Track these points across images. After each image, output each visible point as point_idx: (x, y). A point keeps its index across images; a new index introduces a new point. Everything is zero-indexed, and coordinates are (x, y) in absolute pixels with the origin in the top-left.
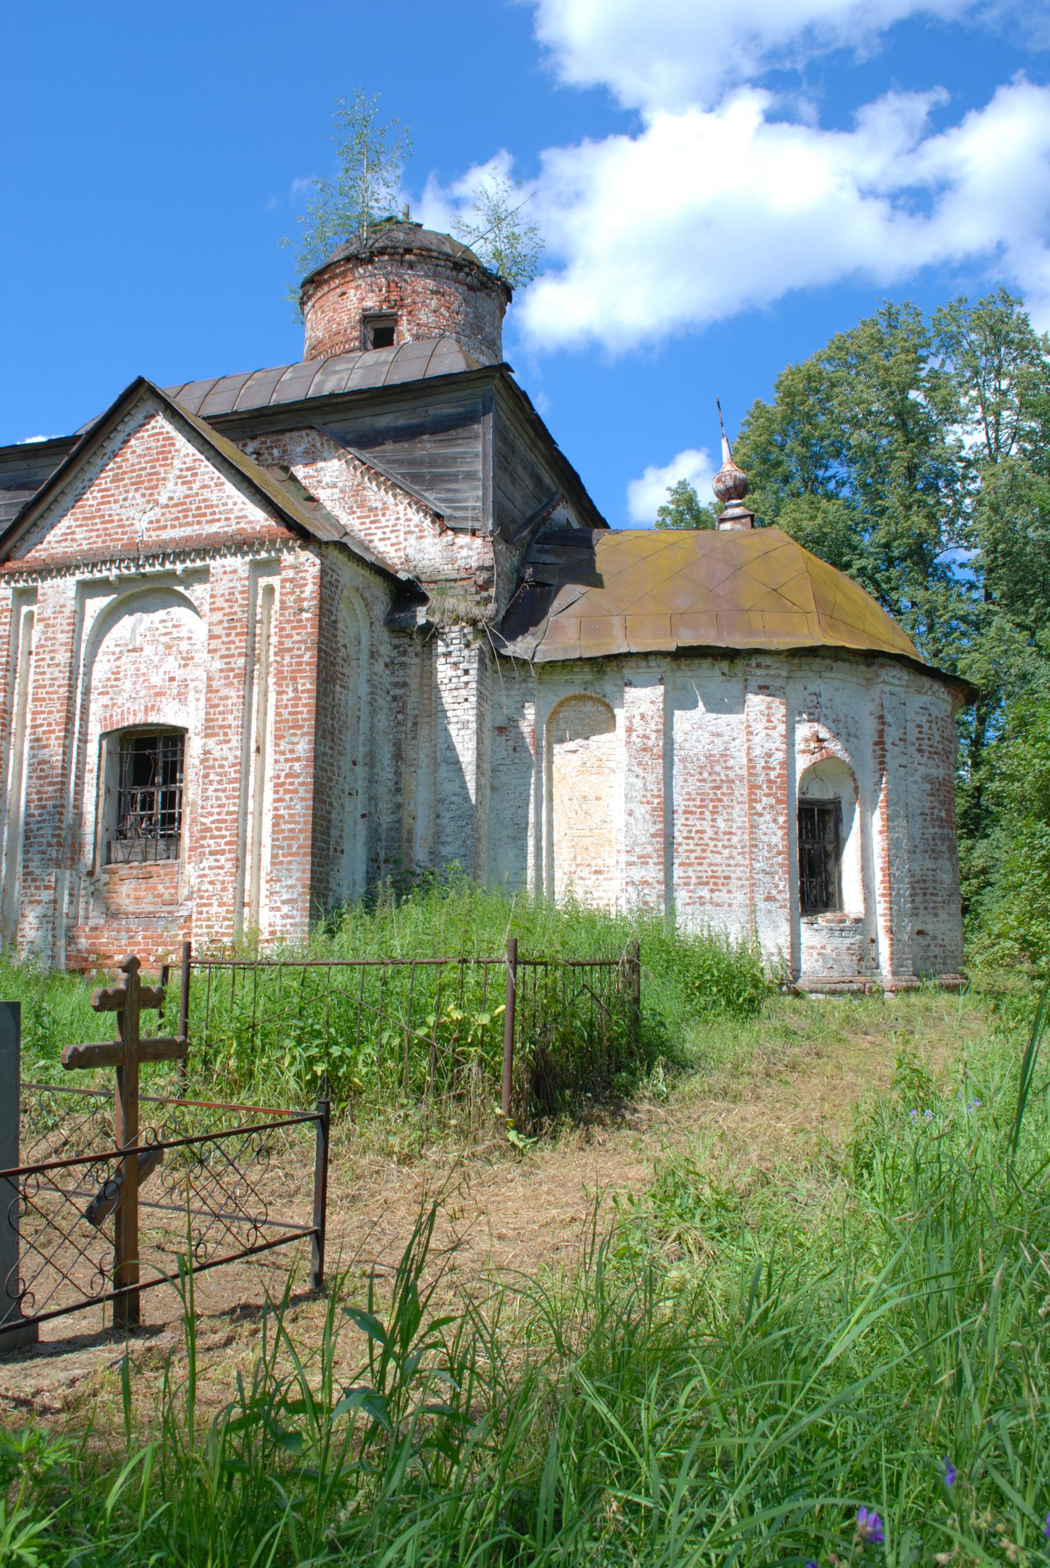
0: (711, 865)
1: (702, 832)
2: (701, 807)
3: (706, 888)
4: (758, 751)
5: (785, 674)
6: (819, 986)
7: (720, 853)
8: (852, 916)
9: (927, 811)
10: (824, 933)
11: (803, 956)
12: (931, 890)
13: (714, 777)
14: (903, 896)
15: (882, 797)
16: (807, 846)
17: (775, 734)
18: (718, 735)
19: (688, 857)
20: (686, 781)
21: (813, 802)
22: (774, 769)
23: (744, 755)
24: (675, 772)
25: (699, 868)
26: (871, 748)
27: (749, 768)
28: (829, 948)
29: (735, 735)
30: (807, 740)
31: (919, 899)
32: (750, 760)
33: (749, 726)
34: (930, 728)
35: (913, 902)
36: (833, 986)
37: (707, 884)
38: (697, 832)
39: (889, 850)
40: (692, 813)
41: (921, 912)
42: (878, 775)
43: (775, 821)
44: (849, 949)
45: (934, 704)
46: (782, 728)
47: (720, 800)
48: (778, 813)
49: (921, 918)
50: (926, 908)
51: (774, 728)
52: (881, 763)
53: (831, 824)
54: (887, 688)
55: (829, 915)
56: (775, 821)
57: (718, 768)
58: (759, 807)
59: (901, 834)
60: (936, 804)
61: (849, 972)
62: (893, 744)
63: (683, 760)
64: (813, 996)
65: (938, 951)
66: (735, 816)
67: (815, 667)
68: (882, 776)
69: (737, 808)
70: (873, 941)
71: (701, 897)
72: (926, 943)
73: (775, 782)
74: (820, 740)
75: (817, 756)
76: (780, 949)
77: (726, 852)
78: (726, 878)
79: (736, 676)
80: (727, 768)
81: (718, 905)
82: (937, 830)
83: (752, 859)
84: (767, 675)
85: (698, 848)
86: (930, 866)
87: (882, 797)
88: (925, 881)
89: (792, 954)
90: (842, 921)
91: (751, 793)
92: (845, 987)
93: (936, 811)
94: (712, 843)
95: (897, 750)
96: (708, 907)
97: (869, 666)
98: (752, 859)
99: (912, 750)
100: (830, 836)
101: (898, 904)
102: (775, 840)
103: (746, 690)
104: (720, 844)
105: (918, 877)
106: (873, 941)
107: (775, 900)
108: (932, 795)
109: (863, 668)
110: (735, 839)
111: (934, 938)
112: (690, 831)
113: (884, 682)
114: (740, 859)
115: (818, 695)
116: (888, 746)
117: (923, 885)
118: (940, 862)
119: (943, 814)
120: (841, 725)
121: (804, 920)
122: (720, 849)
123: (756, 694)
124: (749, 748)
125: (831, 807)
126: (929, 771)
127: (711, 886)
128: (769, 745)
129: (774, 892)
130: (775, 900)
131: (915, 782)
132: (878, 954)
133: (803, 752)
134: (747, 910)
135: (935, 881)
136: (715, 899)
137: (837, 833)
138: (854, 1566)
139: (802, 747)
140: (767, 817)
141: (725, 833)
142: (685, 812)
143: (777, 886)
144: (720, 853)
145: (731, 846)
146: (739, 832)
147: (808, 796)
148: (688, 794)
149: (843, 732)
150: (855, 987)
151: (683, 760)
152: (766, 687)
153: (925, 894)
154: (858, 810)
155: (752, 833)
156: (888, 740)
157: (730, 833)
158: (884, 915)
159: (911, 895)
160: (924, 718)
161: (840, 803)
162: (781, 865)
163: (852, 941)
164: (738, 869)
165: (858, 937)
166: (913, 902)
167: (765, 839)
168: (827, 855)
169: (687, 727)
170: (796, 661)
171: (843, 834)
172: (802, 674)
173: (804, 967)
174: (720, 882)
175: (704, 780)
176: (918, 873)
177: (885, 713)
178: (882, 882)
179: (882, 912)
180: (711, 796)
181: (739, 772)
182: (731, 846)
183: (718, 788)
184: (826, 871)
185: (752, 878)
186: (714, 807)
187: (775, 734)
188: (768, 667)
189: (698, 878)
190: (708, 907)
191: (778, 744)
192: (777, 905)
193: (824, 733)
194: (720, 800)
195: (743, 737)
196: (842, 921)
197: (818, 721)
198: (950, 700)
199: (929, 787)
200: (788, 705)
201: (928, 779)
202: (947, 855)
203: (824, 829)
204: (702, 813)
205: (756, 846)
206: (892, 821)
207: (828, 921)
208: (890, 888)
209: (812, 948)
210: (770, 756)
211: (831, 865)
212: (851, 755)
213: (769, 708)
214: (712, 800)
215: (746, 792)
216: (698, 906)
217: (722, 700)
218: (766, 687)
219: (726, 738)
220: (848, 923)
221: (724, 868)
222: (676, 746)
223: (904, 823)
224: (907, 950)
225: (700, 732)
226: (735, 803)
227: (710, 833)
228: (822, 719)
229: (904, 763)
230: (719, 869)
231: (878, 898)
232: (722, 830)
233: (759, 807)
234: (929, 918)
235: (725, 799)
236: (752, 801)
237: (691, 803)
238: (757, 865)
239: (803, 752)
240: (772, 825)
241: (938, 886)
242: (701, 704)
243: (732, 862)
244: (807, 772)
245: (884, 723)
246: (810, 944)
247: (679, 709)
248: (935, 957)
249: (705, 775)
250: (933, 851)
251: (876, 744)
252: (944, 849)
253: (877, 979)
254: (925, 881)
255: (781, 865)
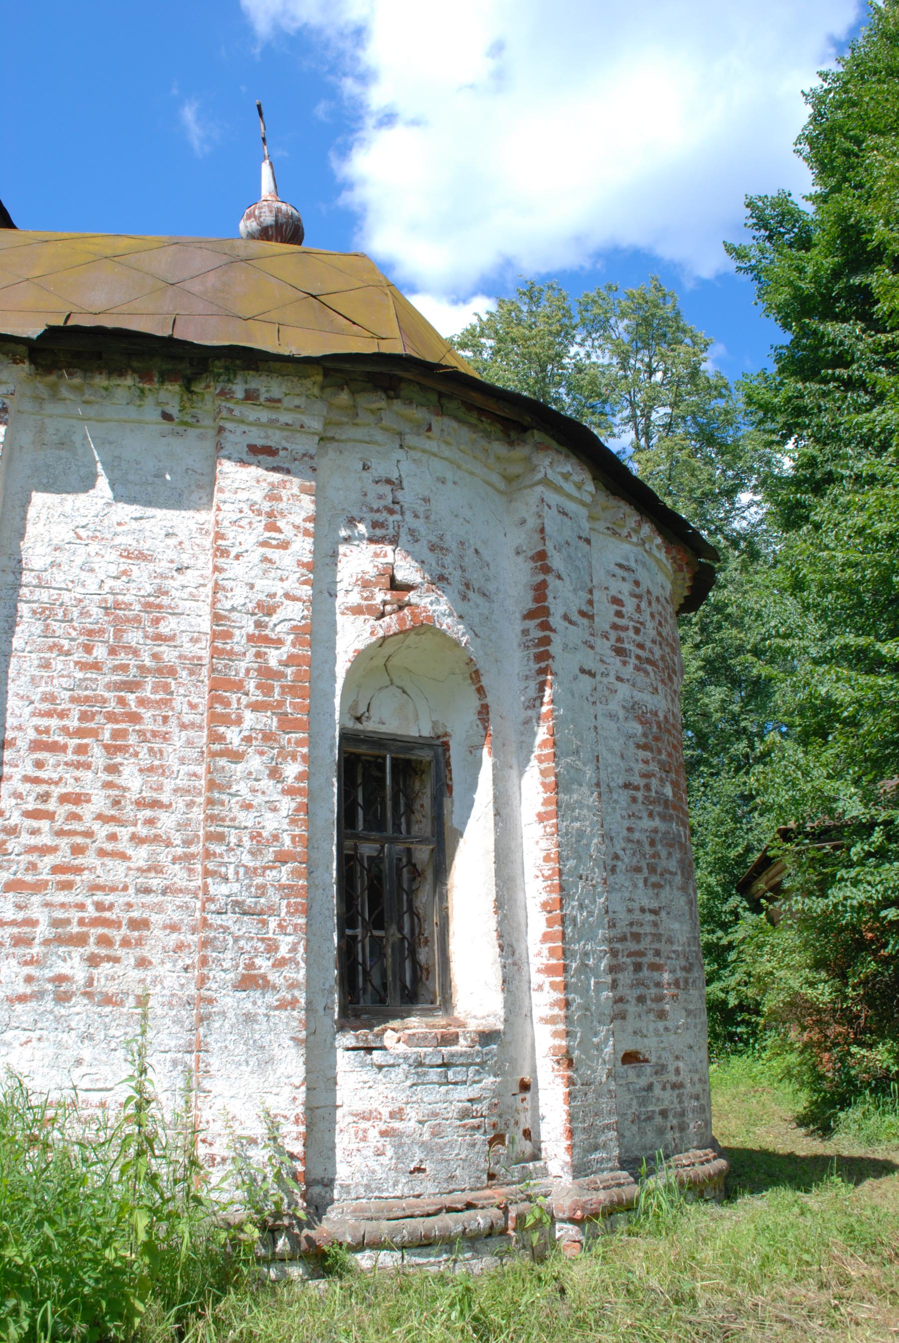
0: (95, 888)
1: (78, 799)
2: (80, 733)
3: (77, 953)
4: (238, 597)
5: (316, 425)
6: (385, 1227)
7: (124, 857)
8: (473, 1025)
9: (637, 780)
10: (397, 1074)
11: (343, 1141)
12: (649, 958)
13: (123, 658)
14: (595, 971)
15: (542, 733)
16: (367, 849)
17: (286, 560)
18: (142, 556)
19: (32, 867)
20: (46, 665)
21: (379, 741)
22: (278, 643)
23: (206, 610)
24: (17, 643)
25: (61, 897)
26: (518, 626)
27: (215, 636)
28: (412, 1114)
29: (186, 559)
30: (366, 585)
31: (625, 978)
32: (217, 618)
33: (219, 536)
34: (638, 609)
35: (614, 985)
36: (421, 1225)
37: (80, 940)
38: (64, 799)
39: (560, 858)
40: (54, 748)
41: (632, 1008)
42: (533, 685)
43: (275, 773)
44: (465, 1114)
45: (644, 564)
46: (303, 547)
47: (135, 718)
48: (285, 754)
49: (631, 1024)
50: (641, 999)
51: (284, 545)
52: (540, 657)
53: (426, 800)
54: (553, 498)
55: (415, 1024)
56: (275, 773)
57: (133, 637)
58: (233, 736)
59: (587, 822)
60: (654, 767)
61: (464, 1177)
62: (566, 617)
63: (44, 613)
64: (364, 1260)
65: (667, 1098)
66: (172, 761)
67: (388, 420)
68: (541, 689)
69: (179, 739)
70: (525, 1087)
71: (60, 979)
72: (643, 1082)
73: (281, 675)
74: (394, 585)
75: (391, 623)
76: (273, 1126)
77: (140, 855)
78: (135, 924)
79: (195, 423)
80: (159, 638)
81: (107, 1000)
82: (657, 823)
83: (207, 873)
84: (272, 423)
85: (64, 843)
86: (646, 903)
87: (542, 733)
88: (637, 937)
89: (308, 1139)
90: (449, 1040)
91: (215, 699)
92: (452, 1223)
93: (654, 782)
94: (102, 831)
95: (576, 635)
96: (79, 1004)
97: (511, 444)
98: (207, 873)
99: (604, 647)
100: (423, 826)
101: (584, 991)
102: (271, 823)
103: (219, 450)
104: (124, 833)
105: (622, 928)
106: (525, 1087)
107: (265, 985)
108: (645, 747)
109: (499, 448)
110: (167, 822)
111: (661, 1069)
112: (44, 797)
113: (546, 482)
114: (177, 874)
115: (396, 484)
116: (556, 621)
117: (633, 946)
118: (665, 893)
119: (668, 791)
120: (448, 560)
121: (348, 1039)
122: (123, 845)
123: (242, 462)
124: (217, 588)
125: (425, 755)
126: (638, 696)
127: (92, 948)
128: (266, 585)
129: (263, 964)
130: (265, 985)
131: (612, 716)
132: (537, 1119)
133: (357, 610)
134: (188, 1016)
135: (657, 937)
136: (101, 985)
137: (439, 819)
138: (520, 1342)
139: (355, 598)
140: (255, 763)
141: (140, 804)
142: (36, 746)
143: (272, 947)
144: (124, 857)
145: (156, 839)
146: (180, 803)
147: (370, 726)
148: (49, 698)
149: (455, 576)
150: (480, 1219)
151: (44, 613)
152: (270, 451)
153: (638, 967)
154: (487, 761)
155: (210, 802)
156: (557, 609)
157: (155, 804)
158: (552, 1020)
159: (612, 969)
160: (627, 587)
161: (446, 746)
162: (286, 890)
163: (473, 1091)
164: (171, 902)
165: (489, 1080)
166: (614, 985)
167: (246, 819)
168: (416, 873)
169: (63, 533)
170: (344, 397)
171: (454, 820)
172: (358, 433)
173: (342, 1172)
174: (117, 935)
175: (96, 666)
176: (623, 917)
177: (549, 547)
178: (546, 938)
179: (547, 1012)
180: (112, 706)
181: (189, 648)
182: (156, 839)
183: (131, 686)
184: (413, 913)
185: (205, 923)
186: (116, 734)
187: (286, 560)
188: (274, 402)
189: (56, 923)
190: (79, 1004)
191: (291, 585)
192: (271, 999)
193: (407, 571)
194: (135, 718)
195: (205, 561)
196: (449, 1040)
197: (394, 541)
198: (669, 565)
199: (639, 729)
200: (319, 495)
201: (634, 710)
202: (678, 879)
203: (410, 809)
204: (81, 750)
205: (220, 838)
206: (568, 791)
207: (411, 1040)
208: (565, 953)
209: (366, 1116)
210: (270, 611)
211: (423, 897)
212: (471, 628)
213: (273, 497)
214: (111, 717)
215: (202, 699)
216: (49, 1003)
217: (160, 475)
218: (270, 451)
219: (162, 566)
220: (462, 1046)
221: (131, 896)
222: (27, 577)
223: (592, 800)
224: (606, 1104)
225: (94, 547)
226: (173, 727)
227: (99, 802)
228: (404, 538)
229: (590, 665)
230: (119, 899)
231: (537, 978)
232: (133, 795)
233: (233, 736)
234: (649, 1023)
235: (147, 714)
236: (216, 719)
237: (54, 723)
238: (219, 890)
239: (357, 610)
240: (266, 783)
241: (663, 947)
242: (103, 482)
243: (155, 882)
244: (361, 658)
245: (546, 569)
246: (359, 1107)
247: (47, 488)
248: (664, 1113)
249: (100, 652)
250: (652, 869)
251: (529, 615)
252: (673, 865)
253: (536, 1185)
254: (637, 937)
255: (286, 890)
